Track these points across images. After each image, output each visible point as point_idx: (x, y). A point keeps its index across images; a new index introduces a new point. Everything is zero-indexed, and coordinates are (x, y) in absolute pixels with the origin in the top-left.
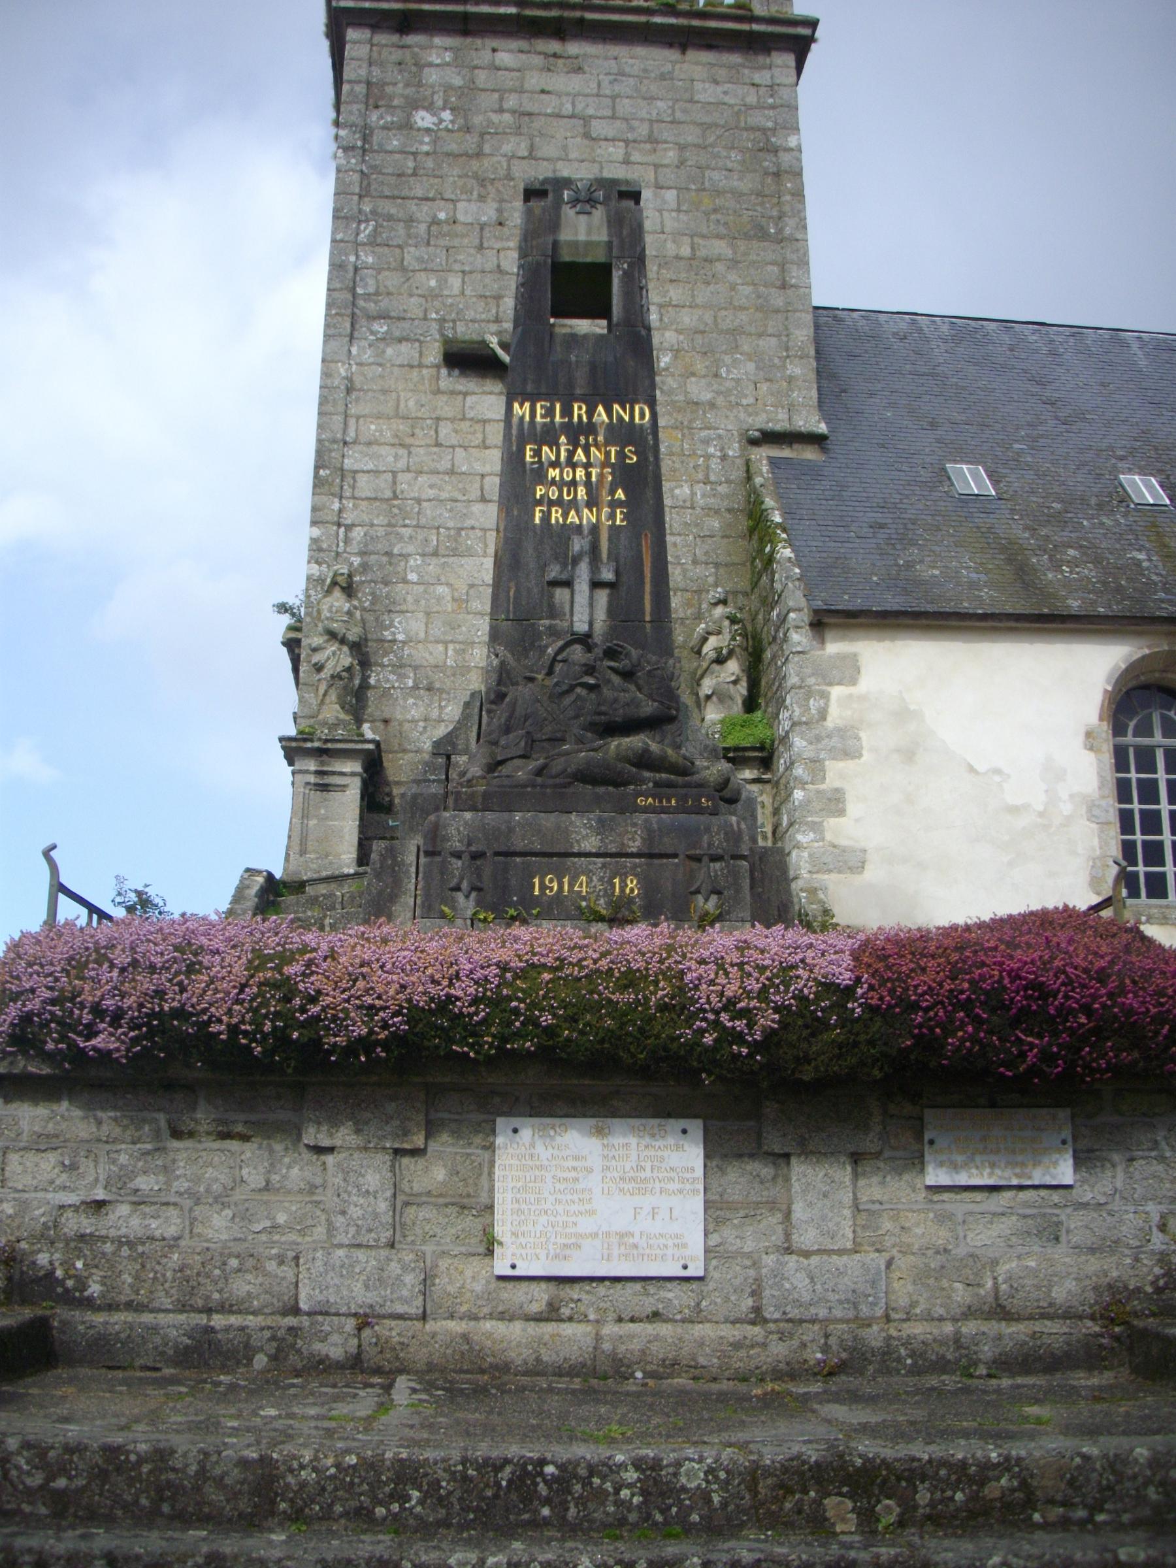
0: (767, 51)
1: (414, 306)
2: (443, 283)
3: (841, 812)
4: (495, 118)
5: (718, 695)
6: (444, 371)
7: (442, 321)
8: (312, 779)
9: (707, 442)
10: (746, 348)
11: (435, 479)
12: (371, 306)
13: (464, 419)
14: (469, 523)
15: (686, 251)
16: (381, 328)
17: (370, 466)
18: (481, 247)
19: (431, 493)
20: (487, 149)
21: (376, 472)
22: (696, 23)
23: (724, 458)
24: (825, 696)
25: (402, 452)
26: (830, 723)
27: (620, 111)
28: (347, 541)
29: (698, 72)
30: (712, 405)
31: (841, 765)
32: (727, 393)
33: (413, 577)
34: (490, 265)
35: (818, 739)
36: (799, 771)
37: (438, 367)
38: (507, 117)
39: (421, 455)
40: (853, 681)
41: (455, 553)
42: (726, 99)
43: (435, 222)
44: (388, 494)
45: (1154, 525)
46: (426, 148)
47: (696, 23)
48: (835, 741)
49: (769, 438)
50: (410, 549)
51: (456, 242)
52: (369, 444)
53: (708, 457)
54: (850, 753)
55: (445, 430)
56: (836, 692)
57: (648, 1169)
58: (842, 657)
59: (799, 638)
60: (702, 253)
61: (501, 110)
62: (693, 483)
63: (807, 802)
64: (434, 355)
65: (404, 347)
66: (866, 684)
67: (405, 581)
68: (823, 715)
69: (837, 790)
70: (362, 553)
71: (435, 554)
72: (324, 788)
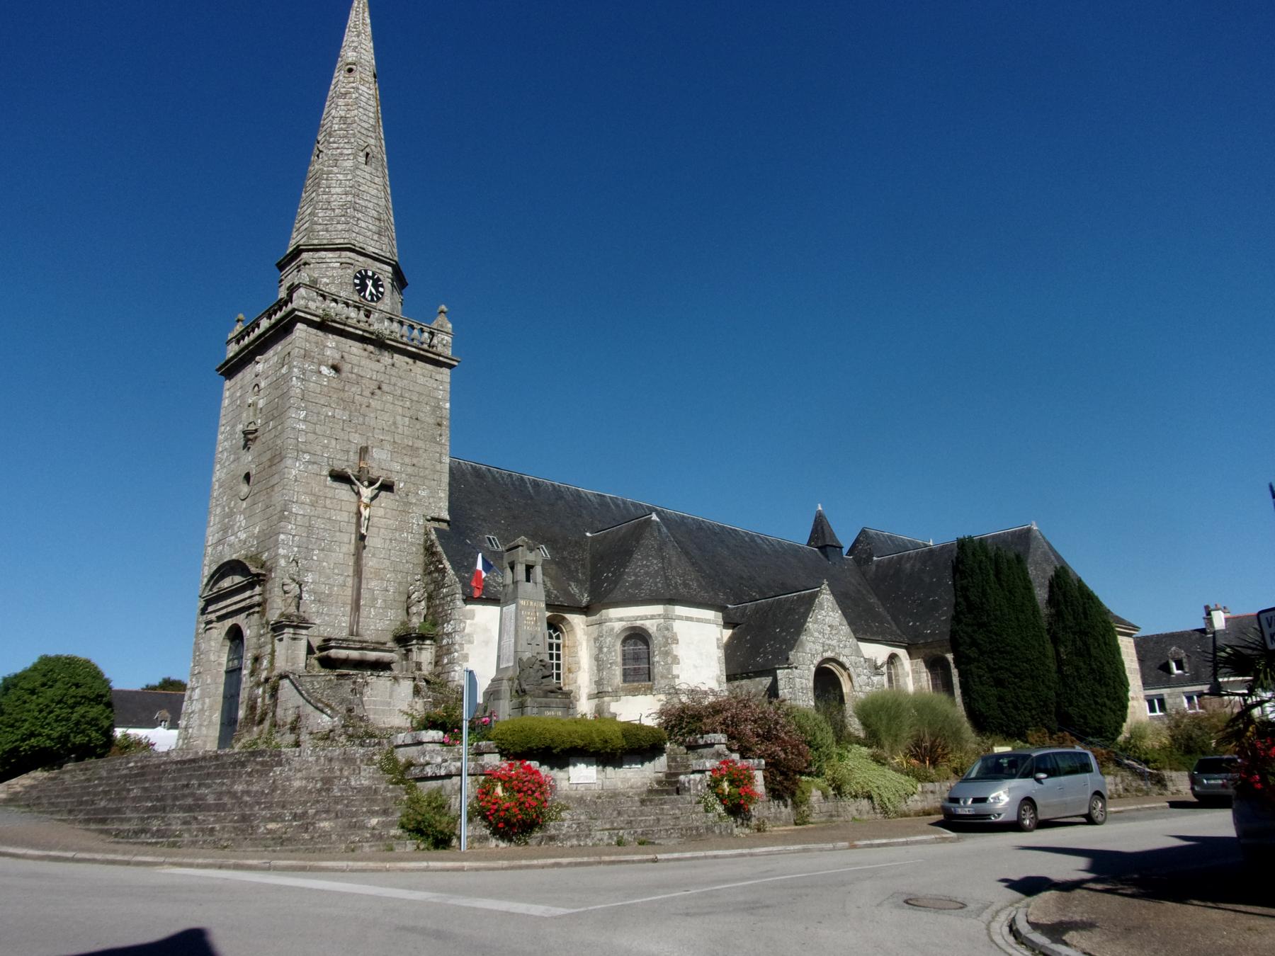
0: (441, 367)
1: (318, 449)
2: (329, 442)
3: (468, 661)
4: (350, 375)
5: (419, 614)
6: (329, 478)
7: (328, 458)
8: (291, 636)
9: (413, 518)
10: (427, 484)
11: (324, 521)
12: (303, 447)
13: (335, 498)
14: (335, 539)
15: (410, 444)
16: (307, 457)
17: (301, 513)
18: (343, 430)
19: (323, 526)
20: (346, 389)
21: (304, 516)
22: (422, 352)
23: (418, 525)
24: (465, 622)
25: (313, 508)
26: (466, 631)
27: (393, 382)
28: (293, 541)
29: (419, 371)
30: (415, 504)
31: (468, 646)
32: (421, 500)
33: (315, 558)
34: (346, 438)
35: (463, 637)
36: (457, 647)
37: (326, 476)
38: (354, 375)
39: (320, 511)
40: (473, 619)
41: (330, 550)
42: (427, 384)
43: (327, 416)
44: (307, 525)
45: (817, 750)
46: (325, 383)
47: (422, 352)
48: (467, 638)
49: (433, 519)
50: (315, 547)
51: (335, 426)
52: (302, 503)
53: (413, 523)
54: (471, 642)
55: (328, 502)
56: (468, 621)
57: (539, 797)
58: (470, 610)
59: (459, 603)
60: (416, 445)
61: (352, 373)
62: (408, 533)
63: (458, 657)
64: (325, 472)
65: (315, 466)
66: (477, 619)
67: (312, 559)
68: (464, 628)
69: (467, 654)
70: (299, 547)
71: (323, 550)
72: (294, 639)
